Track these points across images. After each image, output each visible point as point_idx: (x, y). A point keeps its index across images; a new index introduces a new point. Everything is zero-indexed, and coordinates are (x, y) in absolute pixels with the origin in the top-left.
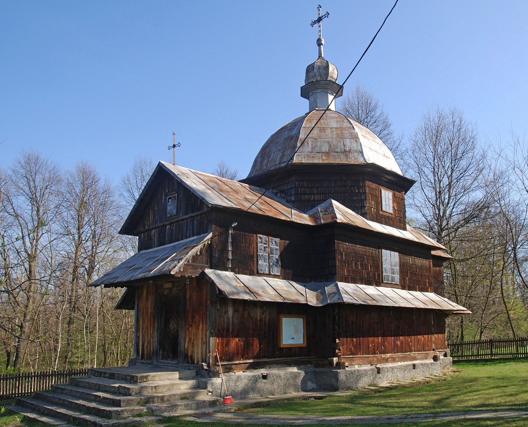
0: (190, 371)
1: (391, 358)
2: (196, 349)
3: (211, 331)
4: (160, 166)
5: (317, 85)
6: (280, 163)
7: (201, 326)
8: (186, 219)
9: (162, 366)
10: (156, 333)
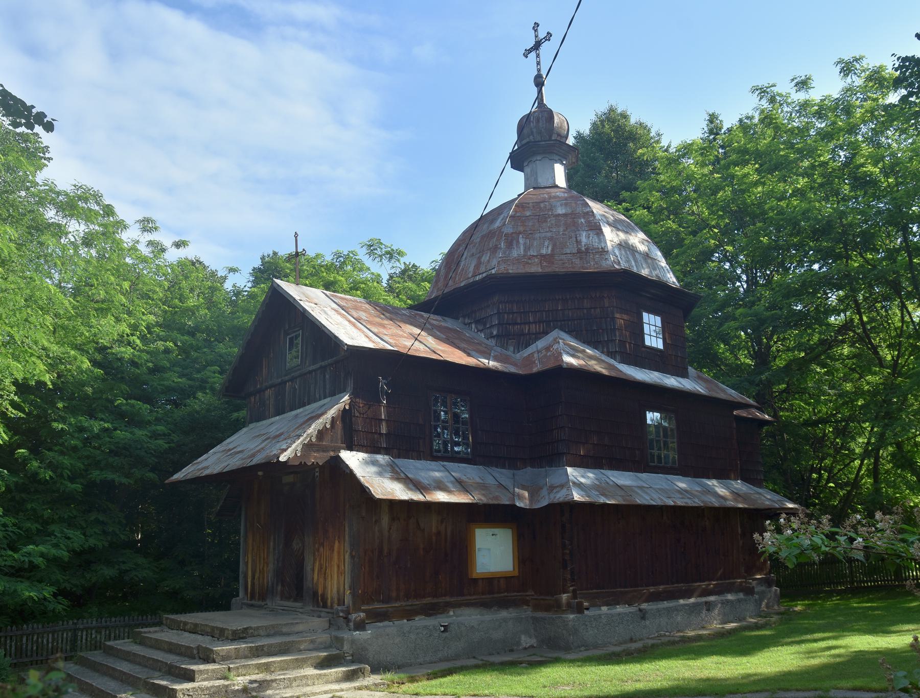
0: (321, 619)
2: (330, 583)
3: (351, 554)
4: (274, 288)
5: (534, 149)
6: (474, 276)
8: (315, 370)
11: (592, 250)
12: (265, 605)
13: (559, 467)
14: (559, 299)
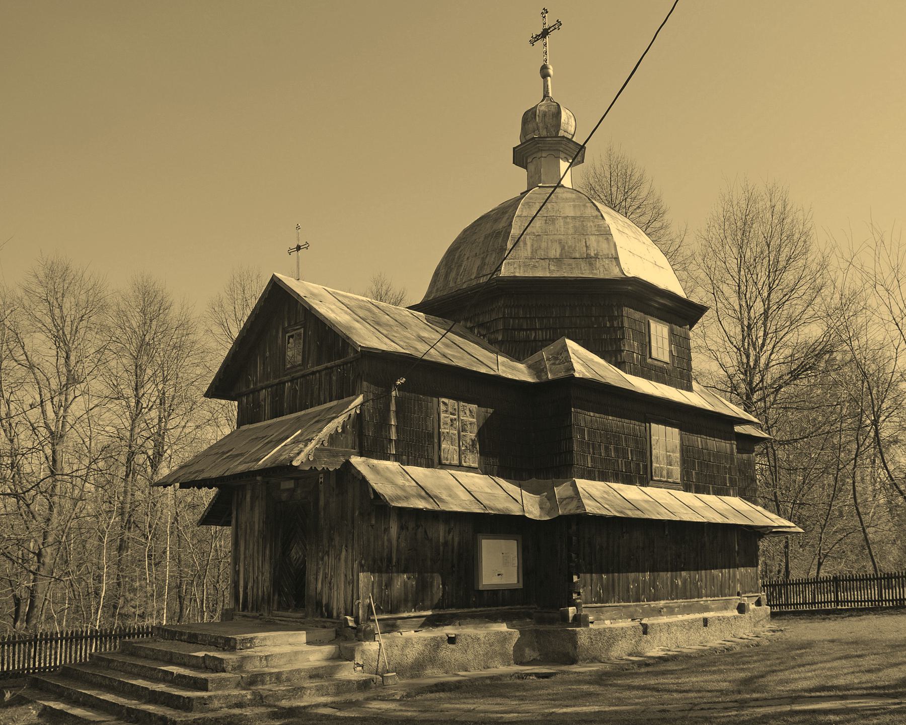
1: (666, 607)
2: (335, 593)
6: (477, 277)
7: (344, 553)
8: (319, 372)
9: (279, 622)
10: (267, 566)
11: (601, 256)
12: (260, 615)
13: (567, 478)
14: (567, 305)
